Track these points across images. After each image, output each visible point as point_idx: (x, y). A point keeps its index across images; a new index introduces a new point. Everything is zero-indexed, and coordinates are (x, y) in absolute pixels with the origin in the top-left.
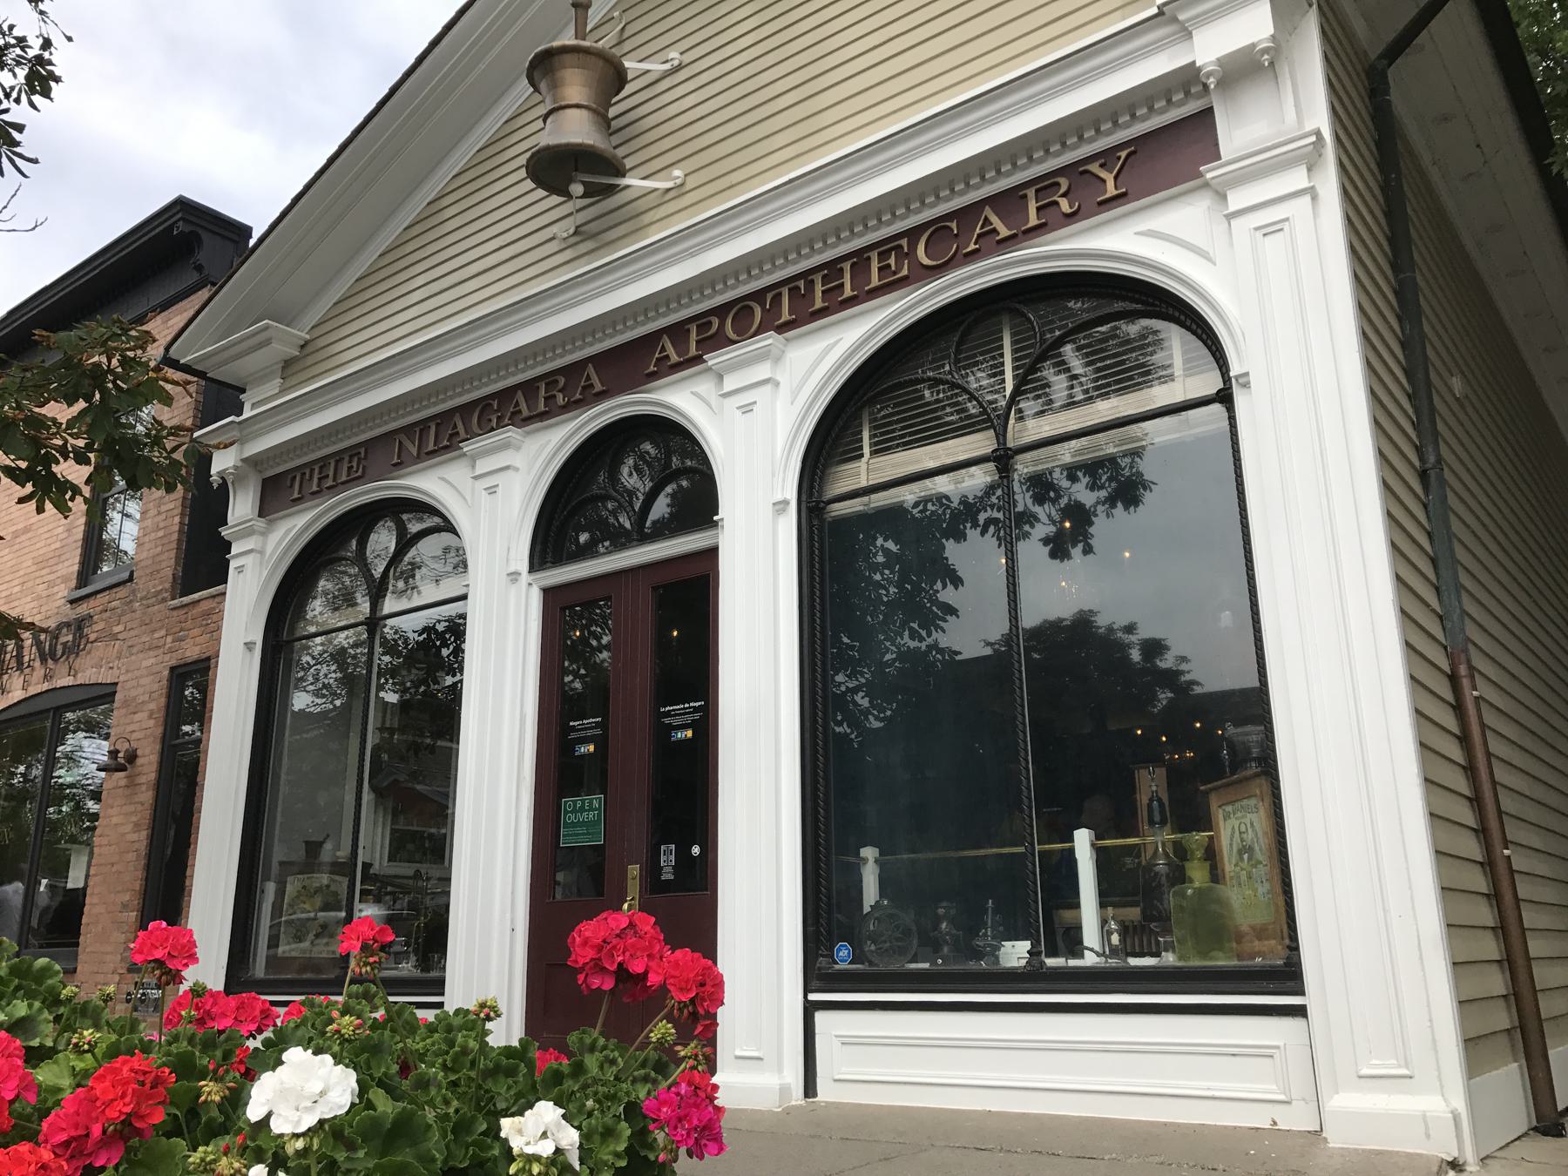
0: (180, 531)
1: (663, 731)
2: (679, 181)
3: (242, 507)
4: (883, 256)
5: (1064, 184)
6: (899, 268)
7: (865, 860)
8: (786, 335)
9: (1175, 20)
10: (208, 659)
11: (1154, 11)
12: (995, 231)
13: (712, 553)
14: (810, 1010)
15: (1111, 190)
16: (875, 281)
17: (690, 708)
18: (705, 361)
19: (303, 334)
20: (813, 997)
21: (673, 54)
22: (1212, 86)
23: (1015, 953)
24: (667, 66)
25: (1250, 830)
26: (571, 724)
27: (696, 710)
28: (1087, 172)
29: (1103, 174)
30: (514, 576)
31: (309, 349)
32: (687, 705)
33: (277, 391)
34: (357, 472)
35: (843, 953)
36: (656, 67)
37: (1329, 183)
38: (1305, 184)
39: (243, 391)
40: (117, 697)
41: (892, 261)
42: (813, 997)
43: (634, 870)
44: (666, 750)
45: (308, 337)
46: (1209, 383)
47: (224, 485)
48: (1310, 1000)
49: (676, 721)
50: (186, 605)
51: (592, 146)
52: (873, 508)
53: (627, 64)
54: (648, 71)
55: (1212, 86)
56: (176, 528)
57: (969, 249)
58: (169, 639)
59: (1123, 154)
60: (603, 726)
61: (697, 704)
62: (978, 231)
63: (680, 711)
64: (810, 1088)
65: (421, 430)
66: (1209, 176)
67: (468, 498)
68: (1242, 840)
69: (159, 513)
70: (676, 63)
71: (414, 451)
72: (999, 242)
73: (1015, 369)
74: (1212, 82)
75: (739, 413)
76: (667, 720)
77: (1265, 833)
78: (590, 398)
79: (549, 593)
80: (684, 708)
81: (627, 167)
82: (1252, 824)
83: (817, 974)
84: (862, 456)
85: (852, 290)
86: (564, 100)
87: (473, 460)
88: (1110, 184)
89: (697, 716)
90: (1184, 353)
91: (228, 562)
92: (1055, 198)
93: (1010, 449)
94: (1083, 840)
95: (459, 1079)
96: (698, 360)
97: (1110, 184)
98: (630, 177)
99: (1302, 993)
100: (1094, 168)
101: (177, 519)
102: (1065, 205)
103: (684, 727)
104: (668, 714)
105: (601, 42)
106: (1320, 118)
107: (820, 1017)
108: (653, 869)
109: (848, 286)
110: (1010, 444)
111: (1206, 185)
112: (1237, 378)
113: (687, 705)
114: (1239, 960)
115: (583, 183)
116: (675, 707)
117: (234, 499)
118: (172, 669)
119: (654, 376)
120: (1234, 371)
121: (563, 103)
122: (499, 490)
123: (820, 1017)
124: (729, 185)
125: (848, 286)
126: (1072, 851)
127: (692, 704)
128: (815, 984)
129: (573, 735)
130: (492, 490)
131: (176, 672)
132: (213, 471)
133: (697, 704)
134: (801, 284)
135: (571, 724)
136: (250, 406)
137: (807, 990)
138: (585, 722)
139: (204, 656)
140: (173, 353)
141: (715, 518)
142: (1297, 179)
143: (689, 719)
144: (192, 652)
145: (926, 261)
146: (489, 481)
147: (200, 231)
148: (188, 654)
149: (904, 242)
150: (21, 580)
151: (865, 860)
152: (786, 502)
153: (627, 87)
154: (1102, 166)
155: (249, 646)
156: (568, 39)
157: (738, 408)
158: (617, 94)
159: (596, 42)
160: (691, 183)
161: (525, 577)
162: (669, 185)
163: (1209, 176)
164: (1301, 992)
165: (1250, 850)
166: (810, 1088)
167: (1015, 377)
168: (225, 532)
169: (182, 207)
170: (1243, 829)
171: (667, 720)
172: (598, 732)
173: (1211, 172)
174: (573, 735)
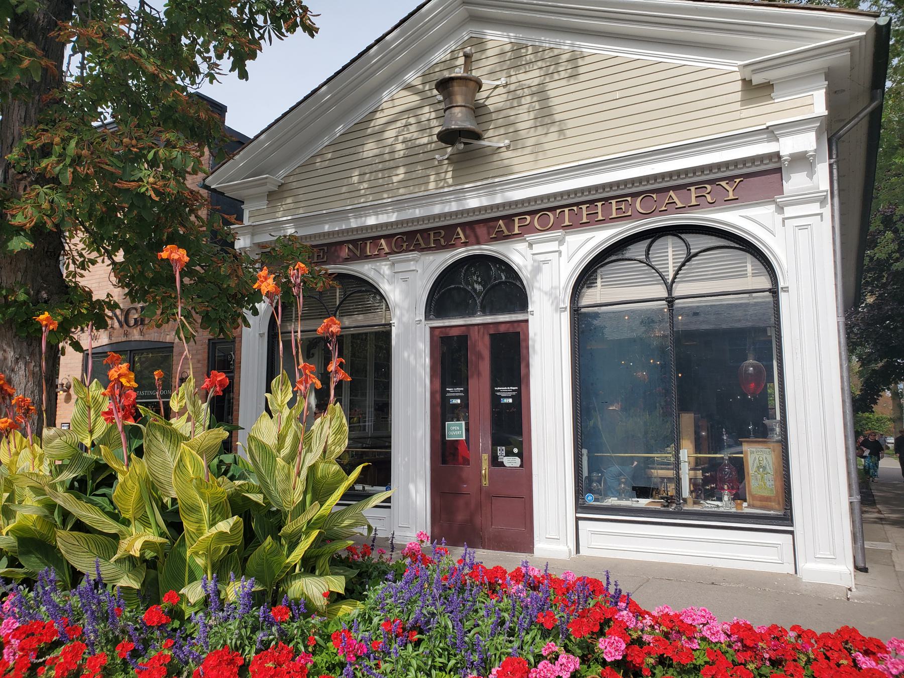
1: (495, 399)
9: (773, 132)
11: (764, 127)
15: (731, 197)
19: (279, 179)
20: (579, 515)
25: (765, 460)
27: (513, 391)
31: (285, 188)
34: (323, 258)
37: (827, 211)
38: (819, 212)
39: (243, 203)
40: (175, 350)
41: (321, 254)
42: (579, 515)
46: (768, 285)
49: (503, 395)
59: (738, 180)
64: (578, 551)
66: (778, 200)
71: (358, 254)
76: (498, 394)
77: (773, 464)
79: (432, 329)
82: (766, 458)
88: (731, 193)
89: (514, 393)
95: (213, 524)
97: (731, 193)
99: (792, 526)
102: (442, 241)
104: (499, 391)
106: (825, 185)
107: (580, 522)
109: (600, 214)
112: (782, 288)
120: (781, 284)
123: (580, 522)
125: (600, 214)
128: (579, 510)
129: (448, 395)
131: (211, 342)
142: (815, 208)
143: (510, 394)
149: (326, 248)
150: (98, 280)
155: (261, 335)
156: (459, 72)
163: (778, 200)
165: (764, 468)
166: (578, 551)
170: (761, 459)
171: (498, 394)
174: (448, 395)
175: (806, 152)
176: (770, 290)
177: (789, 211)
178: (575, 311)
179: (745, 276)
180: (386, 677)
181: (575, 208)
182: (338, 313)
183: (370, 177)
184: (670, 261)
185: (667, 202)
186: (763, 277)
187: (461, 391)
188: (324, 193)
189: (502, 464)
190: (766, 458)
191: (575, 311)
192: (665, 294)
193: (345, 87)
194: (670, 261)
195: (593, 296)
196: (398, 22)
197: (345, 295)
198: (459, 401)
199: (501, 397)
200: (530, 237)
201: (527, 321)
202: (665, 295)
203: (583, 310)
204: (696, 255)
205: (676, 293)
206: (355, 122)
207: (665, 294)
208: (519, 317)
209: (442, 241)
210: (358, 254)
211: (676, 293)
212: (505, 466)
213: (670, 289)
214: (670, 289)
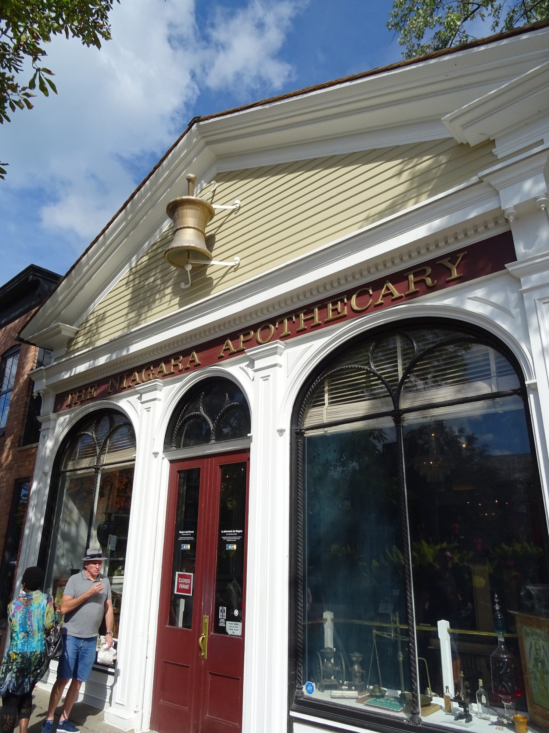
0: (24, 415)
1: (222, 544)
2: (237, 262)
3: (47, 406)
5: (429, 271)
7: (326, 620)
8: (285, 341)
10: (29, 477)
12: (392, 294)
13: (247, 451)
14: (291, 721)
16: (331, 315)
17: (235, 533)
18: (245, 353)
20: (293, 714)
21: (237, 201)
22: (512, 221)
24: (234, 207)
25: (542, 650)
26: (180, 532)
27: (239, 534)
28: (441, 264)
29: (449, 265)
30: (156, 454)
32: (234, 531)
33: (64, 353)
36: (229, 207)
43: (206, 619)
45: (78, 329)
47: (39, 398)
49: (229, 539)
50: (23, 450)
51: (194, 247)
52: (329, 433)
53: (214, 206)
54: (225, 209)
55: (512, 221)
56: (22, 413)
57: (378, 303)
58: (16, 465)
59: (461, 255)
61: (239, 531)
62: (383, 293)
63: (231, 534)
65: (121, 377)
68: (537, 654)
69: (16, 406)
70: (238, 205)
72: (393, 300)
73: (403, 364)
74: (511, 219)
75: (261, 380)
76: (224, 538)
80: (233, 533)
81: (213, 256)
82: (543, 647)
84: (324, 404)
85: (319, 320)
86: (182, 224)
87: (141, 394)
89: (239, 538)
90: (497, 363)
91: (40, 432)
92: (424, 278)
93: (401, 410)
96: (242, 351)
98: (215, 260)
100: (446, 262)
101: (23, 410)
102: (429, 281)
103: (232, 543)
104: (225, 535)
105: (202, 198)
109: (317, 318)
111: (508, 273)
113: (234, 531)
115: (192, 264)
116: (228, 531)
117: (44, 404)
118: (16, 480)
119: (221, 358)
121: (185, 226)
122: (151, 409)
123: (296, 725)
124: (260, 265)
125: (317, 318)
127: (237, 531)
129: (181, 539)
130: (148, 409)
132: (34, 391)
133: (239, 531)
135: (180, 532)
136: (54, 359)
137: (290, 709)
138: (186, 532)
139: (28, 476)
140: (22, 336)
141: (249, 435)
143: (235, 539)
144: (24, 474)
145: (356, 308)
146: (147, 405)
147: (40, 279)
148: (22, 474)
151: (326, 620)
153: (215, 217)
154: (449, 261)
157: (262, 378)
158: (211, 220)
159: (201, 197)
160: (243, 263)
161: (161, 455)
162: (233, 264)
167: (403, 369)
168: (39, 419)
169: (33, 269)
170: (538, 648)
171: (224, 538)
172: (192, 538)
173: (510, 267)
176: (515, 392)
178: (297, 434)
183: (160, 288)
185: (224, 348)
186: (508, 377)
189: (223, 630)
190: (543, 647)
191: (297, 434)
193: (11, 286)
196: (232, 109)
200: (250, 352)
202: (392, 408)
205: (102, 463)
208: (326, 401)
211: (404, 405)
212: (227, 633)
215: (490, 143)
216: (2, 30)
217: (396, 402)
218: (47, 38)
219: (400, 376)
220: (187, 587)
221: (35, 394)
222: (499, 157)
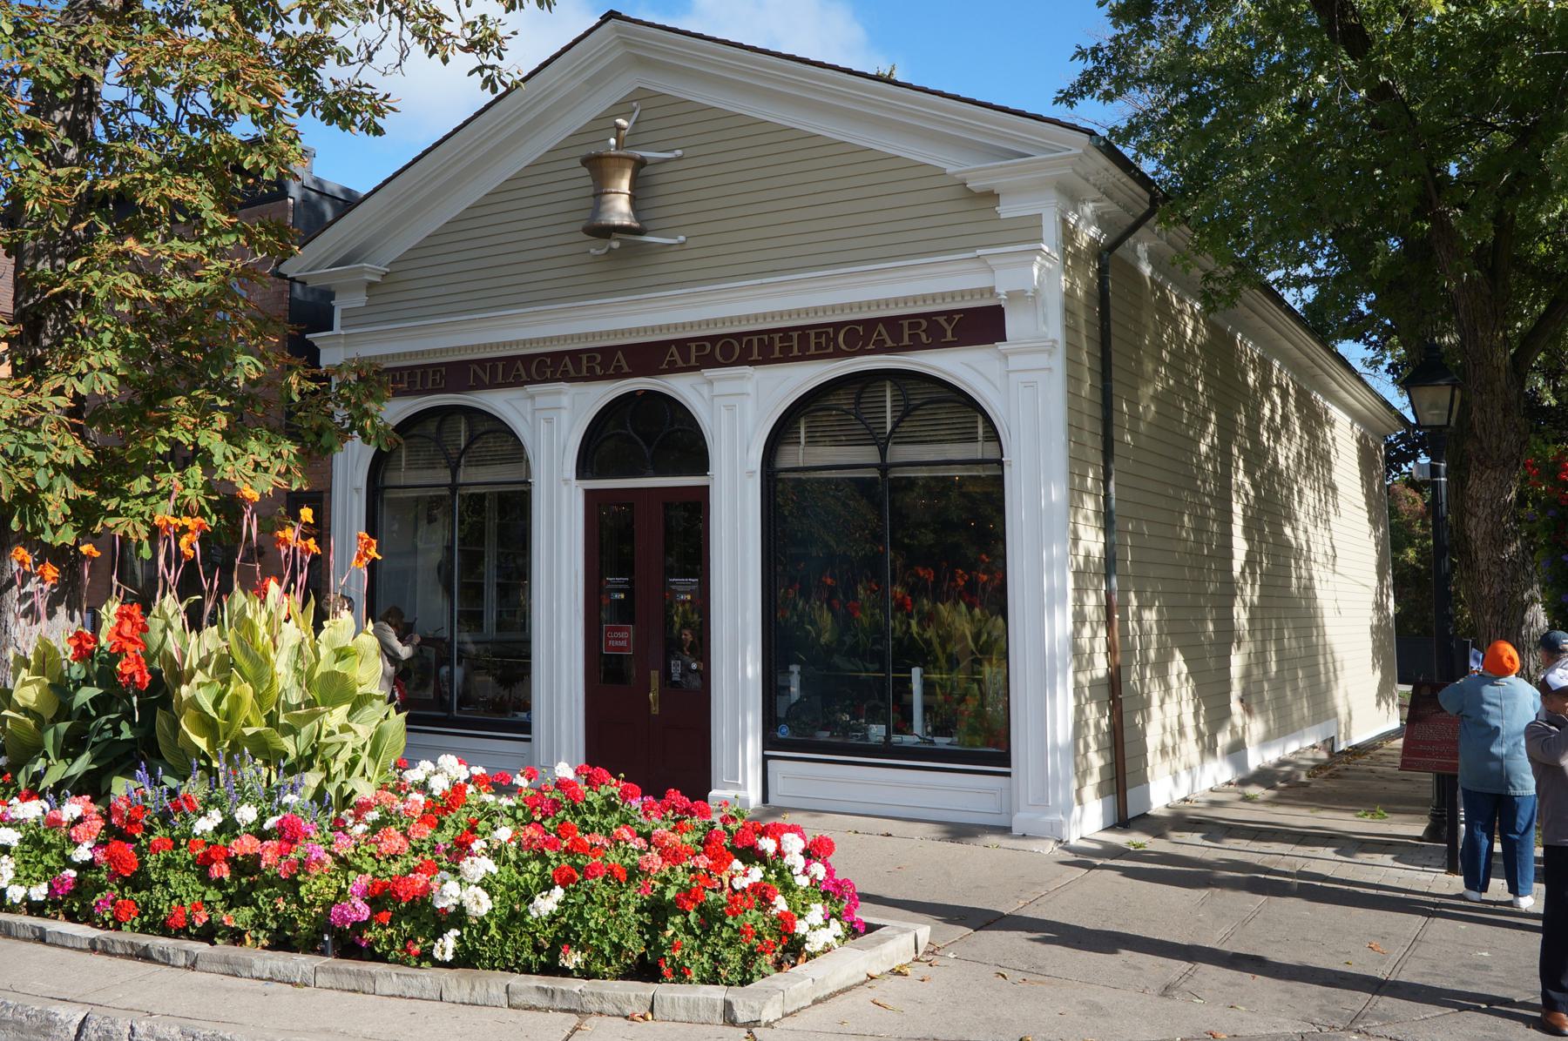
4: (818, 336)
6: (828, 346)
10: (321, 492)
14: (765, 759)
20: (767, 753)
23: (877, 732)
29: (945, 325)
35: (784, 730)
42: (767, 753)
43: (655, 674)
44: (624, 566)
48: (1013, 770)
49: (680, 588)
59: (957, 317)
60: (631, 583)
67: (529, 419)
71: (487, 380)
76: (673, 587)
78: (619, 375)
83: (771, 742)
88: (949, 333)
94: (916, 673)
97: (949, 333)
100: (941, 320)
102: (598, 369)
104: (674, 583)
107: (770, 763)
108: (666, 674)
110: (888, 460)
114: (42, 929)
123: (770, 763)
126: (910, 678)
134: (766, 337)
137: (764, 748)
142: (1041, 360)
145: (843, 347)
152: (754, 472)
164: (1009, 765)
171: (673, 587)
172: (626, 586)
173: (1000, 345)
175: (1024, 291)
177: (1015, 362)
179: (975, 440)
180: (1, 426)
181: (766, 337)
182: (463, 461)
184: (889, 415)
187: (626, 582)
188: (443, 290)
192: (876, 459)
194: (889, 415)
195: (796, 456)
197: (471, 436)
198: (622, 596)
199: (677, 592)
201: (707, 488)
202: (449, 480)
203: (783, 475)
204: (917, 408)
205: (461, 479)
206: (526, 163)
207: (876, 459)
208: (803, 440)
209: (598, 369)
210: (487, 380)
211: (461, 479)
213: (883, 453)
214: (883, 453)
215: (991, 196)
216: (5, 453)
217: (454, 475)
218: (12, 417)
219: (888, 431)
220: (624, 643)
221: (342, 197)
222: (1002, 216)
